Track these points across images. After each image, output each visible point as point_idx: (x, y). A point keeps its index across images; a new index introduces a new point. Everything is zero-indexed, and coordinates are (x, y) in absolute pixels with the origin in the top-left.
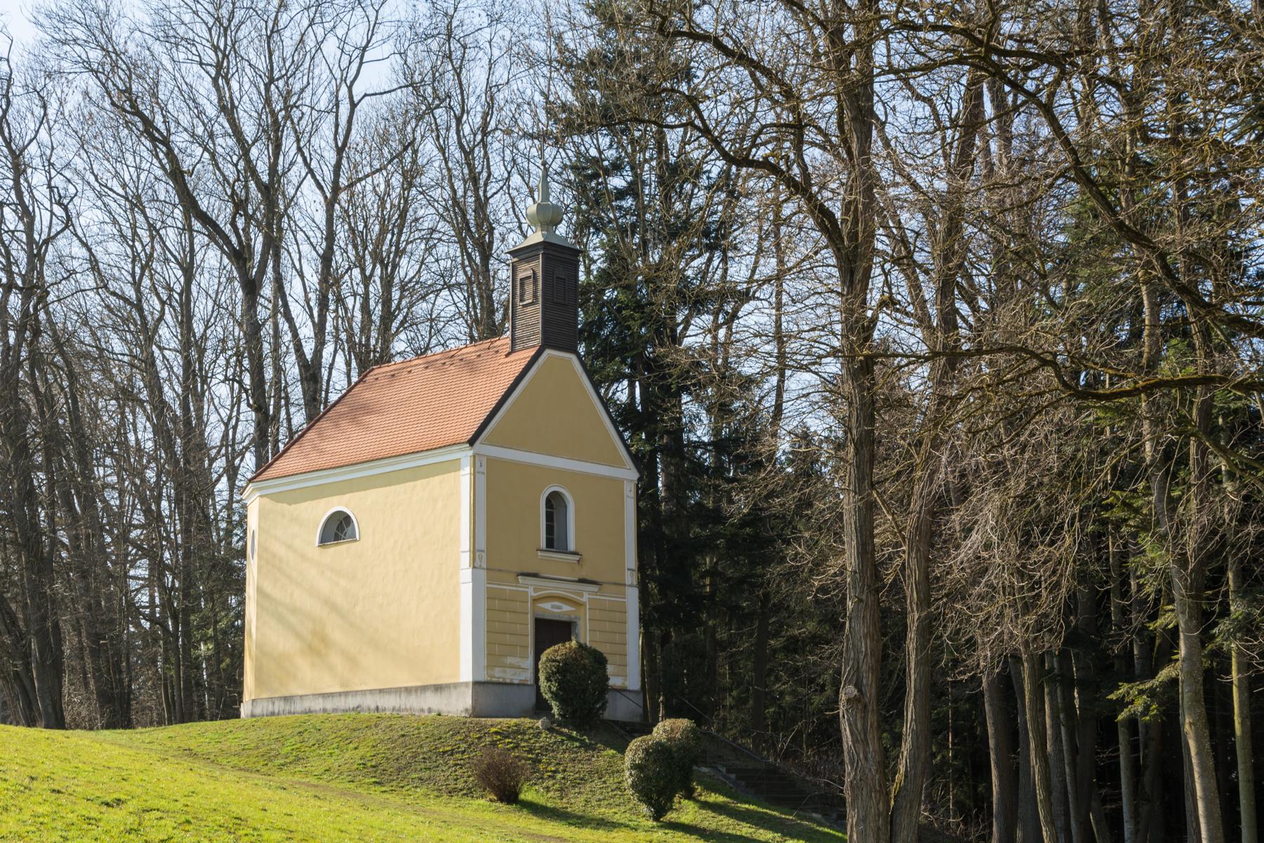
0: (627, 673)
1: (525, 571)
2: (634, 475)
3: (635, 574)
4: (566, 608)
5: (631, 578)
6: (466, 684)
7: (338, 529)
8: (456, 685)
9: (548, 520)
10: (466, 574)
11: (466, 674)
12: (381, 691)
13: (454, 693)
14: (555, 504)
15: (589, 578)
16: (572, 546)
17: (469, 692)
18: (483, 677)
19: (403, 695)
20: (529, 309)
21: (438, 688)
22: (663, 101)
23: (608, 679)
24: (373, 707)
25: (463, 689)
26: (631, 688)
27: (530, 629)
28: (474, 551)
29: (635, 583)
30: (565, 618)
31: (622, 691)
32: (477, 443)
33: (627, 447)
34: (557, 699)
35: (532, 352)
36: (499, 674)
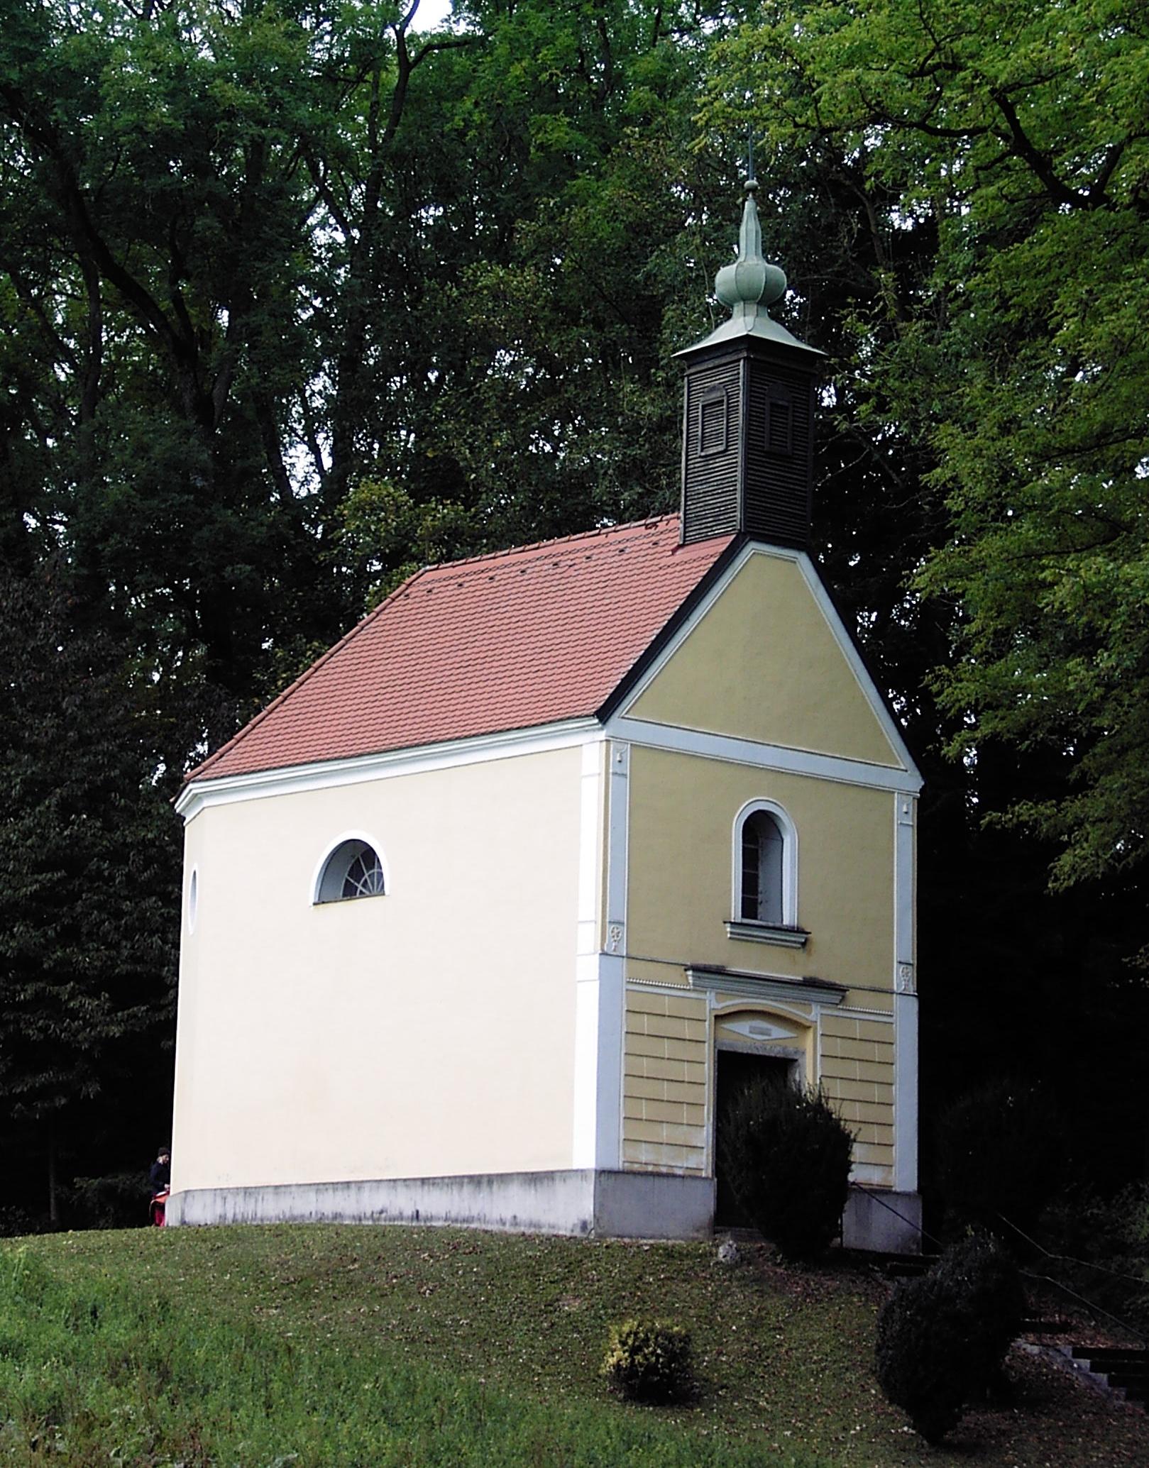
0: (888, 1157)
1: (702, 961)
2: (914, 782)
3: (912, 973)
4: (778, 1032)
5: (902, 978)
6: (581, 1173)
7: (353, 870)
8: (566, 1174)
9: (745, 864)
10: (588, 966)
11: (585, 1157)
12: (424, 1181)
13: (560, 1187)
14: (760, 832)
15: (823, 976)
16: (789, 917)
17: (589, 1187)
18: (617, 1164)
19: (467, 1189)
20: (720, 462)
21: (534, 1179)
22: (1063, 384)
23: (846, 1167)
24: (408, 1212)
25: (574, 1182)
26: (897, 1189)
27: (707, 1072)
28: (608, 923)
29: (912, 989)
30: (776, 1052)
31: (883, 1192)
32: (614, 719)
33: (895, 718)
34: (4, 1339)
35: (722, 544)
36: (645, 1156)
